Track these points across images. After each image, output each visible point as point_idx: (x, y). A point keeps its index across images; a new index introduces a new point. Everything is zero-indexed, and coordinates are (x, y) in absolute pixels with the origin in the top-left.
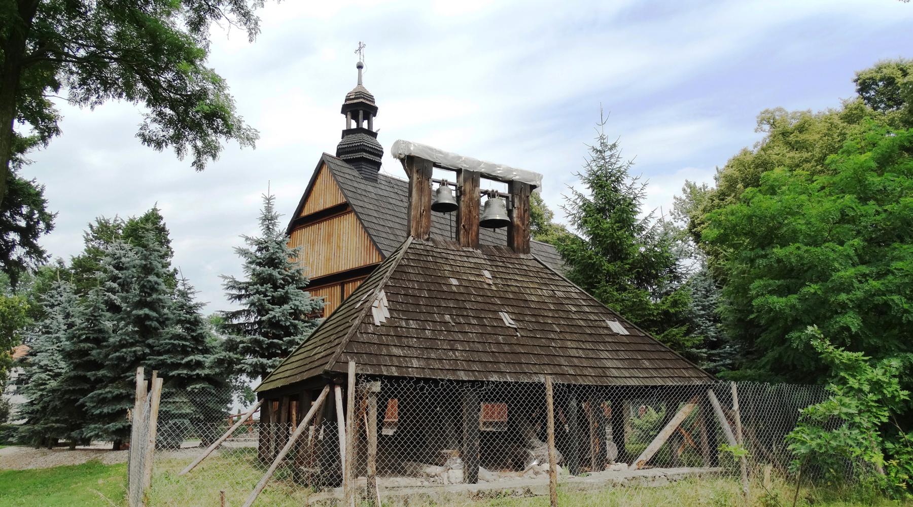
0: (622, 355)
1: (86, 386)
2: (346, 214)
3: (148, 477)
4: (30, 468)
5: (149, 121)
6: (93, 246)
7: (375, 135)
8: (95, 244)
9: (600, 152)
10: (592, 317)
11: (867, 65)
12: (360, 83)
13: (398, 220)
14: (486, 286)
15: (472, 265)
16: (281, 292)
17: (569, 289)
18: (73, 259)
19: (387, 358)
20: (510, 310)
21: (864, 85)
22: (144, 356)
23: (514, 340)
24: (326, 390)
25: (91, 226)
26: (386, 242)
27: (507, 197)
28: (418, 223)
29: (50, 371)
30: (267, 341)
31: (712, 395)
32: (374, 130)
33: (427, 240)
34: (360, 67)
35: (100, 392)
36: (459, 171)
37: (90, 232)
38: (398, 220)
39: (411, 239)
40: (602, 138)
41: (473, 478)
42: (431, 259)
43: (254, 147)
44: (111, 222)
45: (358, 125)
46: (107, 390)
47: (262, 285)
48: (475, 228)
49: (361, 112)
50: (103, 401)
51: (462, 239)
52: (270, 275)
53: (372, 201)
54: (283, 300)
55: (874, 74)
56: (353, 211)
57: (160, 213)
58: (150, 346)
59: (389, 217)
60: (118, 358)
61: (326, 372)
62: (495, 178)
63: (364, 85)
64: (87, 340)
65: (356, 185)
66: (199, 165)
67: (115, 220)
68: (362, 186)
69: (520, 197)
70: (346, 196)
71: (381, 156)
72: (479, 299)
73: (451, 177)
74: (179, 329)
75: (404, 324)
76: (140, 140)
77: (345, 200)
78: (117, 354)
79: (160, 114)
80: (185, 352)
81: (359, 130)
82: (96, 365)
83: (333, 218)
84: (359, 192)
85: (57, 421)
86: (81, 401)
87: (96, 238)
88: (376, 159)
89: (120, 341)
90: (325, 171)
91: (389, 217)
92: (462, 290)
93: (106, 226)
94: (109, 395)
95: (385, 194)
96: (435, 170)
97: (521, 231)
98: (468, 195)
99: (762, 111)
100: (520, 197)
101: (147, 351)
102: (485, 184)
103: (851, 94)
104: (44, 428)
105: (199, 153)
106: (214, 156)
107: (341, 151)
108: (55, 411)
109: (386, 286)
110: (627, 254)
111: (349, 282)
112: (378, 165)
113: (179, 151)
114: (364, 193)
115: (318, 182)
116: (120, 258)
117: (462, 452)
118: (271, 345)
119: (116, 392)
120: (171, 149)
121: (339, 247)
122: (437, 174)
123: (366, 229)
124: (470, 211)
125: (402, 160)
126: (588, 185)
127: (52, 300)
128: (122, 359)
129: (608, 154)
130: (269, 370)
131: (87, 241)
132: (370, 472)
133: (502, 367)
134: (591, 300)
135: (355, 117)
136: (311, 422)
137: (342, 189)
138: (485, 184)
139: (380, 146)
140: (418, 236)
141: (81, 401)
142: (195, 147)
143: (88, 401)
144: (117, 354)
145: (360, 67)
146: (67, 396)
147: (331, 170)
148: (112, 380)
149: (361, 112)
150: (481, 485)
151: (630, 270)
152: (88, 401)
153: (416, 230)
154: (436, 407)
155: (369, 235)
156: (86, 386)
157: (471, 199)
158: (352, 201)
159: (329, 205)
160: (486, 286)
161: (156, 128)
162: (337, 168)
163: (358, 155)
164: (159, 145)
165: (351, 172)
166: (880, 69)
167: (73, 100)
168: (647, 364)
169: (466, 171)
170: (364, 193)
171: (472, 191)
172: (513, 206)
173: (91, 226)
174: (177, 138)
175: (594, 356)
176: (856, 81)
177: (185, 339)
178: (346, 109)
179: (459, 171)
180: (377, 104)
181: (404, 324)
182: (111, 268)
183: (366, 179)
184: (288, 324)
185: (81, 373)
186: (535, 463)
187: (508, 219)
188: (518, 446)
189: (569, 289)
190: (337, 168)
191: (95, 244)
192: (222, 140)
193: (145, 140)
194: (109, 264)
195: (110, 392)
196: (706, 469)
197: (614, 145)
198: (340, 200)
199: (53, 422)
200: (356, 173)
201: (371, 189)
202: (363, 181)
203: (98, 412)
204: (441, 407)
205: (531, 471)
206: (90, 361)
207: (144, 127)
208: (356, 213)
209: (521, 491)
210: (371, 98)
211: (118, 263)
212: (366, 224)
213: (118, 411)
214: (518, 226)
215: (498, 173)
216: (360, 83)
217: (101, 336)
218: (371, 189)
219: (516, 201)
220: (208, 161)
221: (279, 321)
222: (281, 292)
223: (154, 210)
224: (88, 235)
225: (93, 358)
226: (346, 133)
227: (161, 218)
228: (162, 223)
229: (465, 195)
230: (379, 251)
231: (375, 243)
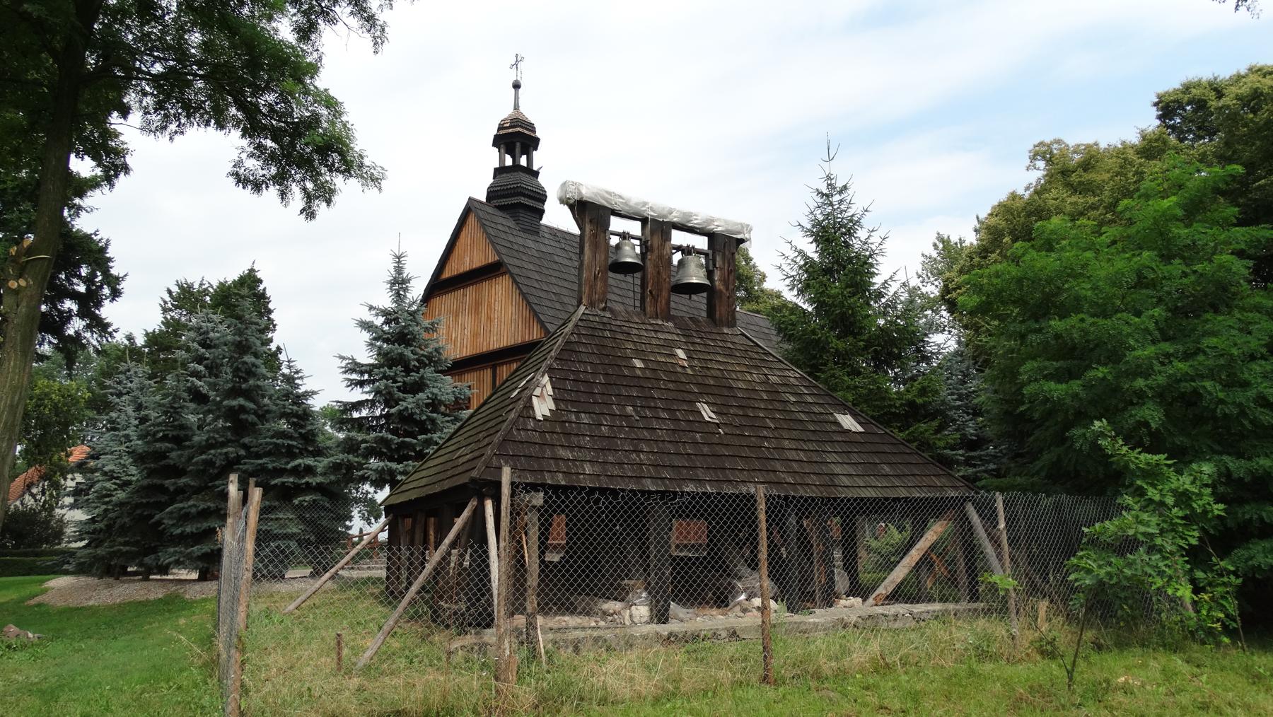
0: (855, 458)
1: (164, 498)
2: (498, 276)
3: (243, 615)
4: (91, 603)
5: (244, 156)
6: (172, 318)
7: (536, 174)
8: (176, 314)
9: (827, 196)
10: (816, 409)
11: (1171, 82)
12: (516, 107)
13: (566, 284)
14: (679, 370)
15: (662, 343)
16: (414, 376)
17: (787, 373)
18: (147, 334)
19: (552, 462)
20: (711, 399)
21: (1167, 108)
22: (238, 460)
23: (716, 439)
24: (473, 503)
25: (170, 292)
26: (551, 313)
27: (706, 255)
28: (592, 288)
29: (117, 478)
30: (396, 440)
31: (971, 510)
32: (535, 168)
33: (604, 309)
34: (517, 86)
35: (181, 505)
36: (644, 221)
37: (168, 299)
38: (566, 284)
39: (582, 308)
40: (829, 178)
41: (661, 616)
42: (608, 334)
43: (380, 189)
44: (196, 286)
45: (514, 161)
46: (191, 503)
47: (390, 368)
48: (665, 294)
49: (518, 145)
50: (185, 517)
51: (648, 309)
52: (401, 355)
53: (532, 260)
54: (418, 387)
55: (1181, 96)
56: (507, 272)
57: (259, 275)
58: (245, 447)
59: (554, 281)
60: (205, 462)
61: (473, 480)
62: (692, 230)
63: (522, 109)
64: (165, 438)
65: (511, 238)
66: (309, 213)
67: (201, 285)
68: (520, 241)
69: (724, 254)
70: (498, 253)
71: (543, 201)
72: (671, 386)
73: (635, 228)
74: (283, 425)
75: (573, 418)
76: (232, 180)
77: (497, 258)
78: (204, 457)
79: (260, 147)
80: (291, 454)
81: (516, 167)
82: (178, 472)
83: (482, 281)
84: (516, 247)
85: (125, 544)
86: (157, 517)
87: (176, 307)
88: (537, 205)
89: (207, 440)
90: (472, 220)
91: (554, 281)
92: (648, 374)
93: (189, 292)
94: (193, 510)
95: (550, 250)
96: (613, 219)
97: (725, 298)
98: (656, 252)
99: (1036, 143)
100: (724, 254)
101: (242, 452)
102: (678, 238)
103: (1150, 121)
104: (109, 553)
105: (309, 197)
106: (329, 202)
107: (492, 194)
108: (123, 530)
109: (550, 370)
110: (861, 328)
111: (502, 364)
112: (541, 213)
113: (283, 195)
114: (522, 249)
115: (463, 234)
116: (207, 333)
117: (649, 584)
118: (403, 445)
119: (202, 506)
120: (272, 192)
121: (489, 318)
122: (616, 224)
123: (524, 295)
124: (659, 273)
125: (571, 207)
126: (811, 239)
127: (120, 388)
128: (210, 463)
129: (836, 198)
130: (399, 478)
131: (165, 310)
132: (529, 609)
133: (701, 474)
134: (816, 387)
135: (510, 151)
136: (453, 545)
137: (493, 243)
138: (678, 238)
139: (542, 189)
140: (591, 304)
141: (157, 517)
142: (304, 189)
143: (165, 517)
144: (204, 457)
145: (517, 86)
146: (139, 512)
147: (479, 219)
148: (197, 491)
149: (518, 145)
150: (673, 626)
151: (866, 348)
152: (165, 517)
153: (590, 296)
154: (615, 525)
155: (529, 303)
156: (164, 498)
157: (660, 257)
158: (506, 259)
159: (476, 265)
160: (679, 370)
161: (252, 164)
162: (488, 217)
163: (514, 200)
164: (257, 186)
165: (504, 222)
166: (1187, 88)
167: (146, 128)
168: (887, 469)
169: (654, 220)
170: (522, 249)
171: (662, 246)
172: (714, 265)
173: (170, 292)
174: (281, 179)
175: (818, 459)
176: (1156, 104)
177: (291, 438)
178: (499, 141)
179: (644, 221)
180: (538, 134)
181: (573, 418)
182: (196, 345)
183: (524, 231)
184: (424, 417)
185: (157, 481)
186: (743, 597)
187: (707, 282)
188: (721, 576)
189: (787, 373)
190: (488, 217)
191: (176, 314)
192: (338, 180)
193: (239, 181)
194: (193, 341)
195: (194, 506)
196: (963, 605)
197: (845, 188)
198: (491, 258)
199: (121, 544)
200: (511, 223)
201: (531, 244)
202: (522, 234)
203: (179, 531)
204: (621, 525)
205: (738, 608)
206: (169, 466)
207: (238, 164)
208: (512, 276)
209: (724, 634)
210: (532, 127)
211: (205, 340)
212: (524, 289)
213: (205, 531)
214: (721, 291)
215: (695, 222)
216: (516, 107)
217: (182, 433)
218: (531, 244)
219: (718, 259)
220: (321, 207)
221: (412, 414)
222: (414, 376)
223: (252, 271)
224: (165, 302)
225: (172, 462)
226: (499, 172)
227: (260, 281)
228: (261, 287)
229: (652, 251)
230: (542, 324)
231: (536, 314)
